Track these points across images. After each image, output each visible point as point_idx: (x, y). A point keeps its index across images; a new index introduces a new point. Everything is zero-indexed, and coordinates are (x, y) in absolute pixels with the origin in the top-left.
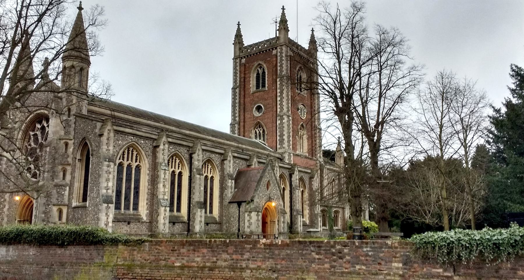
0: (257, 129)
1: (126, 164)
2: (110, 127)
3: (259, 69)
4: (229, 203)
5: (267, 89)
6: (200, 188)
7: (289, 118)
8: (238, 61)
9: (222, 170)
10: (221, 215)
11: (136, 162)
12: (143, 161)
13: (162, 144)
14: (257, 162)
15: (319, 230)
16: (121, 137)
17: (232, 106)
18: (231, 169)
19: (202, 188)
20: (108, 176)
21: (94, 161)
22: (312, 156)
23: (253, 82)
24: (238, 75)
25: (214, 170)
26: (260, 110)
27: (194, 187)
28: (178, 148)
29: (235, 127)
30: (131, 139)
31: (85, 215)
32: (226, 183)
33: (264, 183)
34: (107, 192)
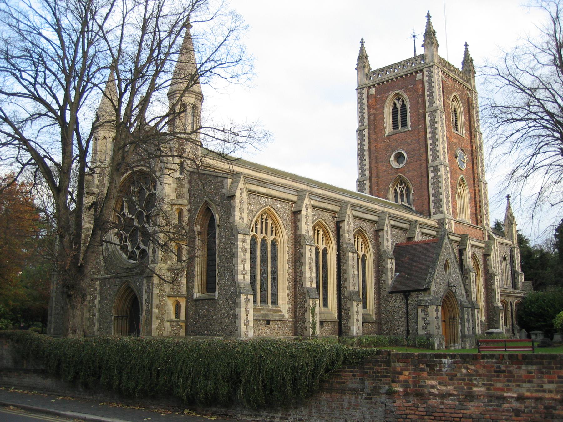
0: (397, 186)
1: (260, 237)
2: (242, 185)
3: (396, 102)
4: (390, 293)
5: (410, 129)
6: (353, 272)
7: (446, 170)
8: (365, 91)
9: (378, 245)
10: (379, 311)
11: (271, 235)
12: (280, 232)
13: (304, 209)
14: (420, 233)
15: (501, 330)
16: (254, 199)
17: (359, 155)
18: (390, 244)
19: (356, 272)
20: (244, 255)
21: (222, 234)
22: (477, 224)
23: (388, 120)
24: (366, 111)
25: (365, 246)
26: (401, 159)
27: (345, 270)
28: (322, 214)
29: (364, 184)
30: (265, 202)
31: (214, 310)
32: (384, 263)
33: (441, 264)
34: (244, 277)
